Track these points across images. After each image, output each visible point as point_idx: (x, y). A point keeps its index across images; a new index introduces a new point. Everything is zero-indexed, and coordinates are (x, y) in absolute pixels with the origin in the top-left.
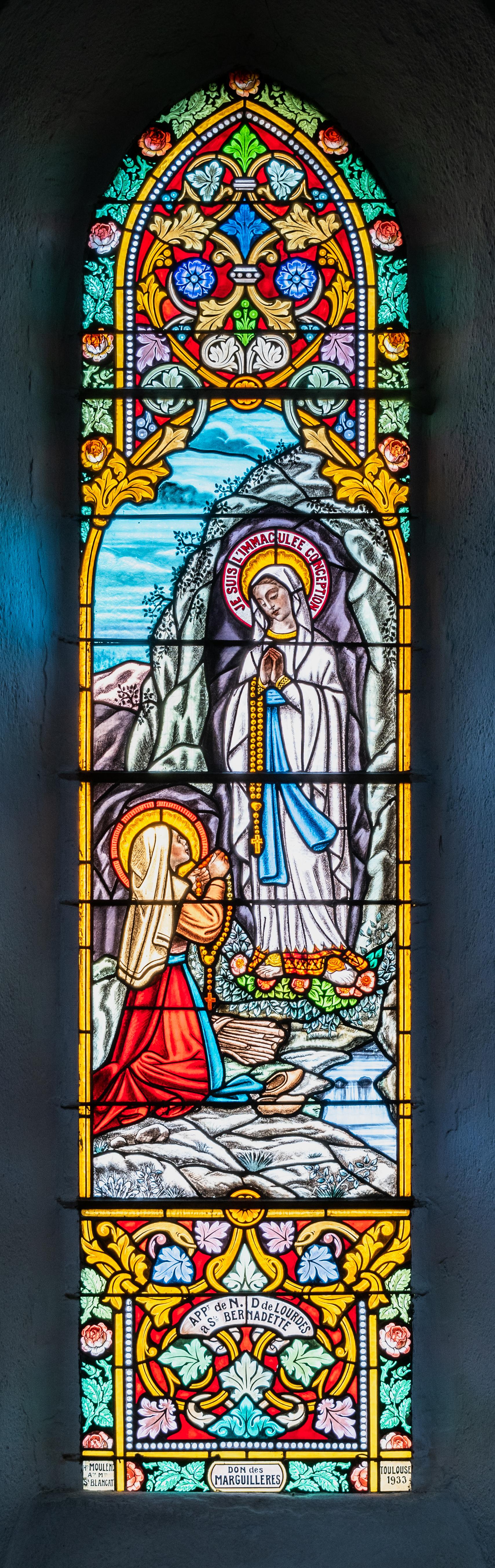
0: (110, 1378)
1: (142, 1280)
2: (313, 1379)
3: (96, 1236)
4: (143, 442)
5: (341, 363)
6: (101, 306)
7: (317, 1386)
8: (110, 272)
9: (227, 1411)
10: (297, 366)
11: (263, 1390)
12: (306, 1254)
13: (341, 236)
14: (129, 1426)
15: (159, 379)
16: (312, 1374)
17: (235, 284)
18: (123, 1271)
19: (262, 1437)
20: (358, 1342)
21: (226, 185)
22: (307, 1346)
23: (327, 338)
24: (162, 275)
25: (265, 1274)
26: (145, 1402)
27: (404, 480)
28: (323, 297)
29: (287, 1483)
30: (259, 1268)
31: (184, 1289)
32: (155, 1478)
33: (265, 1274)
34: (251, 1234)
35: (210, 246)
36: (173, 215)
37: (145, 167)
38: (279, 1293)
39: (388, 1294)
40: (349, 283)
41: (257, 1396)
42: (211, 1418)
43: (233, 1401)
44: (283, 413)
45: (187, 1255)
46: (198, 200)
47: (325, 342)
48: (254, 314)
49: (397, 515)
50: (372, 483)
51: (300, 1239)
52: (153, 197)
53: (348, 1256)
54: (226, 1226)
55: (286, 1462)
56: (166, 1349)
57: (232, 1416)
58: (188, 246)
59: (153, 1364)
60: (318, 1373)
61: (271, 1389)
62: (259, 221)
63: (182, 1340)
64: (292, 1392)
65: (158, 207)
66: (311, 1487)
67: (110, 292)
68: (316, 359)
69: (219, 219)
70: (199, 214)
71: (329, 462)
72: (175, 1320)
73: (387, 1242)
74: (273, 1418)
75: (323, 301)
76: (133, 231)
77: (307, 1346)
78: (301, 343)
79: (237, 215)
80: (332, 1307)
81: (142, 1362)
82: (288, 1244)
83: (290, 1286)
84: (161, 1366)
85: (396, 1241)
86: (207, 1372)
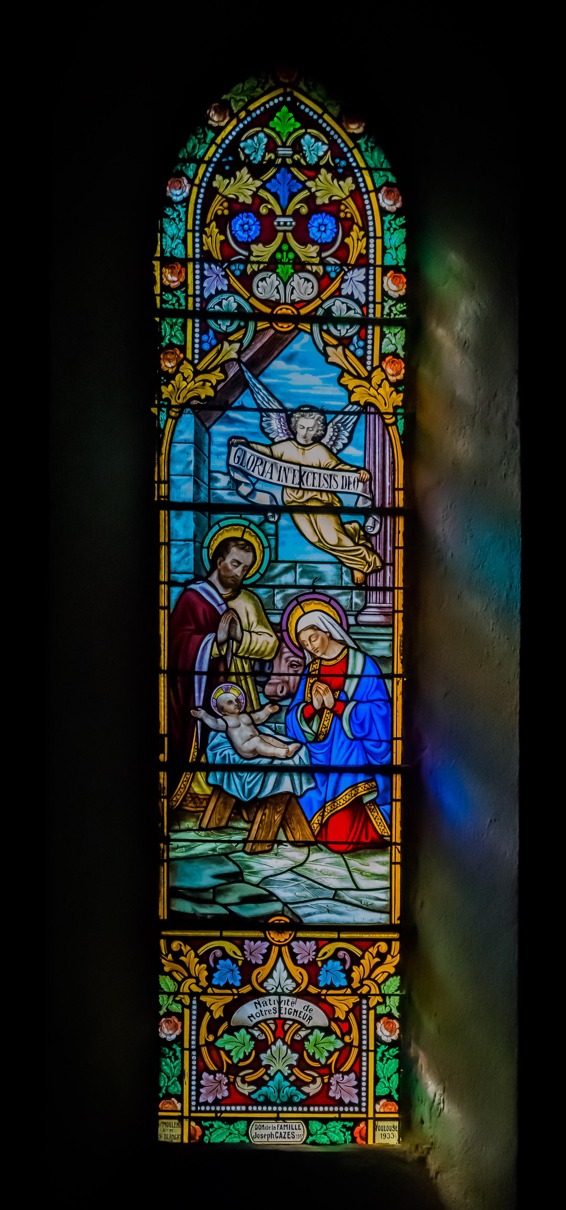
0: (180, 1057)
1: (204, 983)
2: (328, 1058)
5: (356, 297)
6: (176, 243)
7: (331, 1063)
8: (182, 216)
11: (291, 1067)
12: (325, 966)
13: (357, 194)
14: (193, 1093)
18: (190, 976)
20: (360, 1030)
22: (323, 1034)
23: (346, 277)
24: (223, 222)
25: (294, 980)
26: (205, 1075)
27: (401, 389)
28: (343, 243)
29: (307, 1138)
30: (290, 976)
31: (235, 991)
32: (210, 1133)
33: (294, 980)
34: (285, 950)
35: (257, 201)
36: (229, 175)
37: (211, 135)
38: (304, 995)
39: (384, 996)
40: (362, 233)
41: (287, 1072)
43: (269, 1075)
44: (311, 334)
45: (237, 965)
47: (343, 281)
49: (395, 414)
50: (377, 390)
51: (320, 955)
52: (215, 160)
54: (267, 944)
55: (306, 1121)
56: (222, 1036)
57: (268, 1086)
58: (241, 200)
61: (297, 1066)
62: (295, 181)
63: (232, 1030)
65: (219, 169)
66: (325, 1140)
67: (182, 234)
68: (337, 294)
70: (249, 175)
71: (345, 374)
72: (230, 1009)
73: (383, 957)
74: (299, 1089)
76: (199, 186)
77: (323, 1034)
78: (326, 281)
79: (278, 175)
80: (342, 1005)
81: (203, 1046)
82: (311, 957)
83: (312, 990)
84: (218, 1049)
85: (389, 958)
86: (250, 1054)
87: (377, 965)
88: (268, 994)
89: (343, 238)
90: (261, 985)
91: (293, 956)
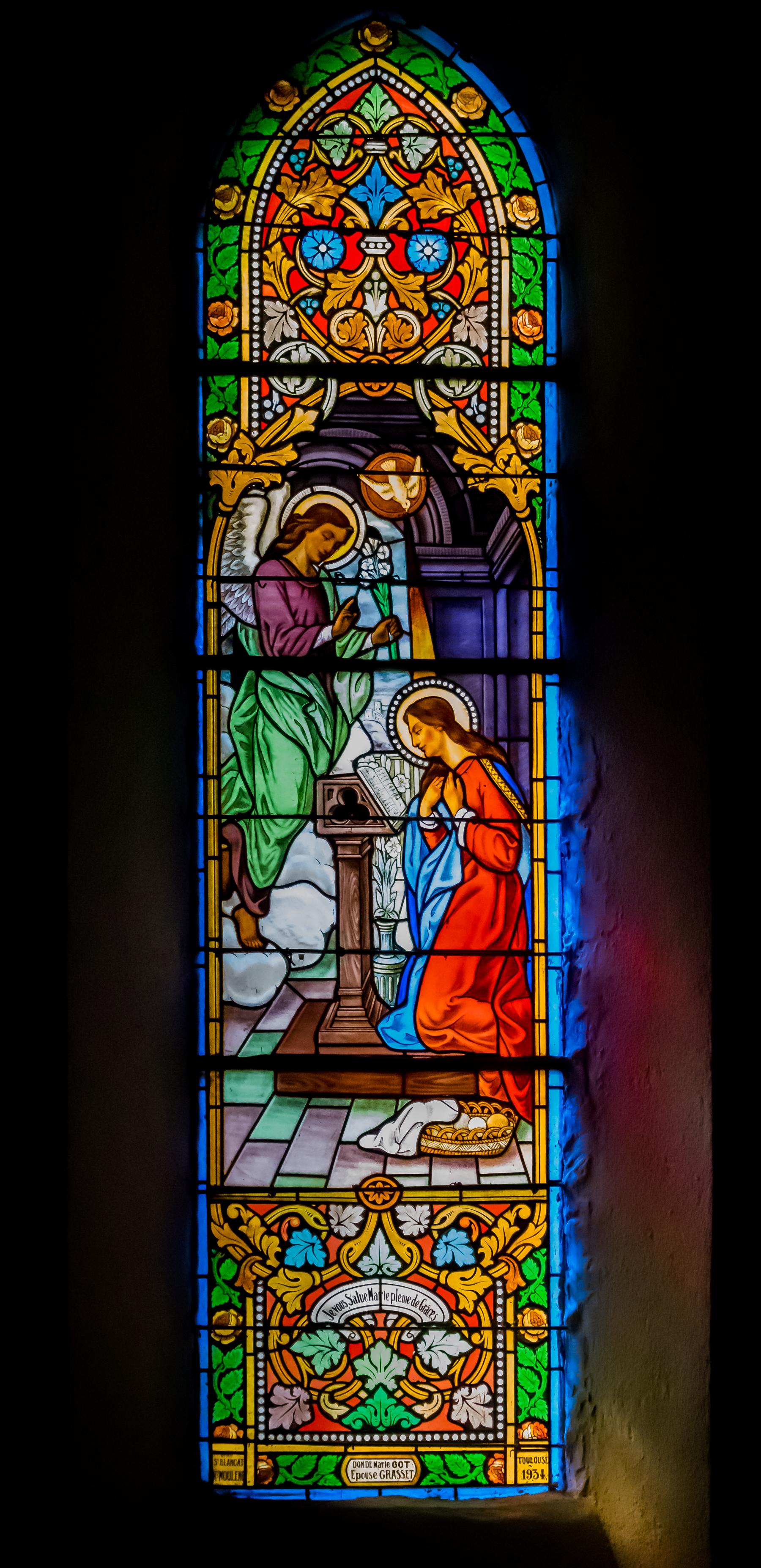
1: (273, 1262)
2: (450, 1367)
3: (226, 1218)
4: (270, 423)
5: (473, 345)
7: (454, 1374)
9: (363, 1402)
10: (429, 346)
11: (398, 1379)
15: (288, 355)
16: (449, 1362)
17: (366, 255)
19: (396, 1428)
21: (356, 147)
25: (398, 1258)
28: (455, 272)
30: (393, 1252)
33: (398, 1258)
34: (386, 1219)
35: (340, 212)
41: (391, 1385)
42: (344, 1410)
43: (367, 1390)
46: (328, 162)
47: (455, 322)
48: (384, 286)
53: (484, 1241)
54: (360, 1210)
59: (285, 1353)
60: (454, 1359)
63: (313, 1328)
64: (429, 1381)
68: (448, 339)
69: (350, 184)
73: (522, 1224)
74: (409, 1409)
75: (455, 276)
83: (425, 1270)
85: (531, 1226)
87: (516, 1236)
88: (366, 1277)
89: (457, 264)
90: (354, 1266)
91: (397, 1223)
